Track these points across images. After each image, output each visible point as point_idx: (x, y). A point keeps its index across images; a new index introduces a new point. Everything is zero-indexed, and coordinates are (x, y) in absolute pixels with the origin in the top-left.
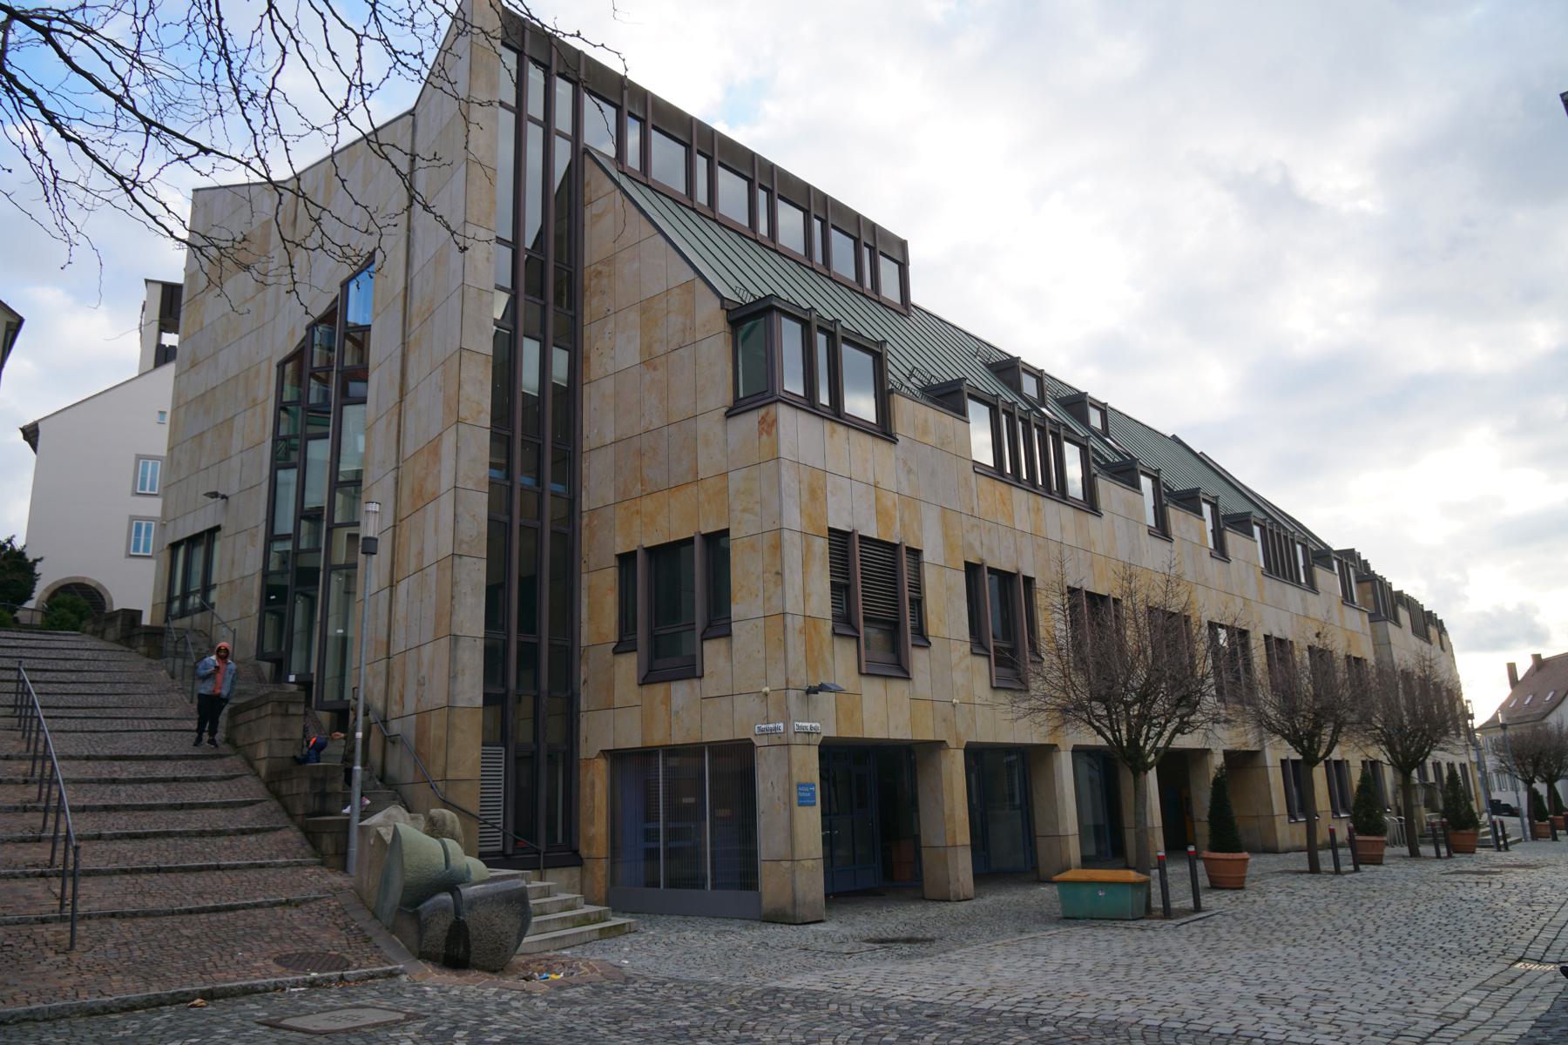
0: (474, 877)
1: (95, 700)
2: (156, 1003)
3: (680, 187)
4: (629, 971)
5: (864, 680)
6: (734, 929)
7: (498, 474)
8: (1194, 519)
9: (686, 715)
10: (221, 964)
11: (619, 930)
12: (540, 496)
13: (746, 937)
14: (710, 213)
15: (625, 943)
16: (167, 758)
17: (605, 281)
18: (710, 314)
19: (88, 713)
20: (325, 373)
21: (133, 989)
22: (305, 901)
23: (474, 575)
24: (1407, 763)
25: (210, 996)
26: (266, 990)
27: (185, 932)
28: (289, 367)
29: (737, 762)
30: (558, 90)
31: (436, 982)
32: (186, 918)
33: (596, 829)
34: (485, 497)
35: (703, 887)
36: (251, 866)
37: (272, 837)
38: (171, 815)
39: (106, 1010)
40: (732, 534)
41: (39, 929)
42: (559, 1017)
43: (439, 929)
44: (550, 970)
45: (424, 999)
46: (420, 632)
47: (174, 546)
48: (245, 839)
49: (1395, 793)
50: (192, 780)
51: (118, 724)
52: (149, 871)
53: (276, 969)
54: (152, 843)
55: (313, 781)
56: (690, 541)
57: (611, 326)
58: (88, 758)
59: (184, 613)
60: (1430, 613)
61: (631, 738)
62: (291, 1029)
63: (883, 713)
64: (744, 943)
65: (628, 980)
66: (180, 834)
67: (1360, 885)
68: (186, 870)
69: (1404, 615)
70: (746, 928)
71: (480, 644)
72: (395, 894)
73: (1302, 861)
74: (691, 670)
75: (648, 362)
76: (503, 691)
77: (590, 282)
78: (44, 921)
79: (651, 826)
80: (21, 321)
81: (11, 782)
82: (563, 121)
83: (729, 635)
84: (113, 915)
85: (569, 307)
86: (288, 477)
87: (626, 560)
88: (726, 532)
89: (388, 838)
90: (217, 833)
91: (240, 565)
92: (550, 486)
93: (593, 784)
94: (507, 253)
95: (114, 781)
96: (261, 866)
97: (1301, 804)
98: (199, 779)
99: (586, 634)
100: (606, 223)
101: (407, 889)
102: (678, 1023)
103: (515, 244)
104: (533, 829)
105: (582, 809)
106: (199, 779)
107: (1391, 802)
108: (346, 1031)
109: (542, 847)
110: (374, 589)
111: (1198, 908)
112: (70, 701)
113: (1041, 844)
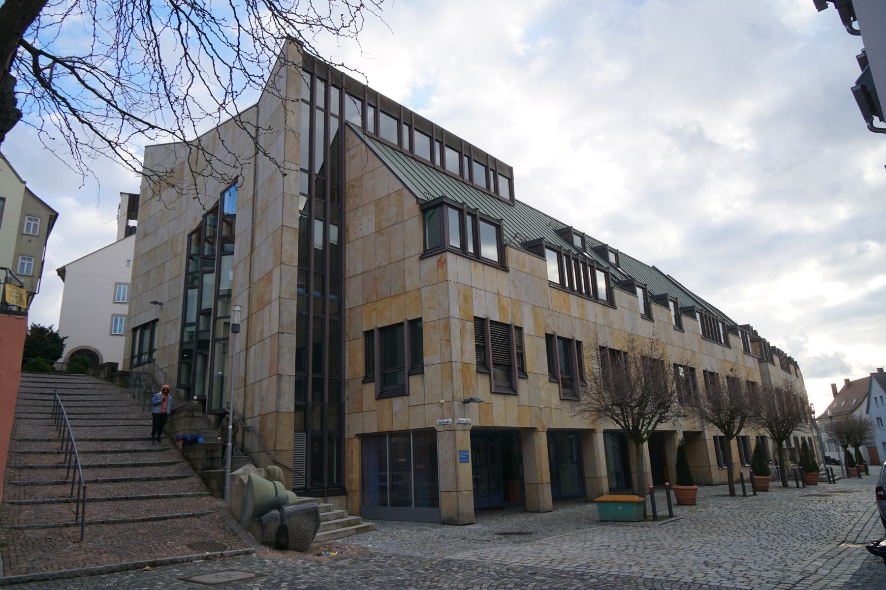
0: (291, 501)
2: (125, 569)
4: (372, 551)
5: (493, 396)
7: (302, 290)
9: (400, 415)
11: (366, 529)
13: (433, 532)
14: (410, 154)
15: (370, 536)
16: (131, 440)
18: (411, 205)
20: (212, 239)
22: (203, 514)
23: (290, 343)
24: (780, 437)
25: (153, 565)
26: (183, 562)
27: (141, 531)
28: (194, 236)
31: (271, 557)
32: (141, 524)
33: (354, 475)
34: (295, 302)
35: (410, 506)
36: (174, 496)
37: (185, 481)
38: (133, 469)
39: (100, 572)
41: (65, 530)
42: (336, 575)
43: (272, 528)
44: (330, 550)
45: (265, 566)
46: (262, 373)
47: (135, 330)
48: (171, 482)
49: (774, 453)
51: (106, 423)
52: (122, 499)
53: (187, 550)
54: (123, 484)
55: (207, 451)
56: (402, 324)
57: (360, 213)
58: (90, 440)
59: (139, 364)
60: (790, 358)
62: (195, 582)
63: (504, 413)
64: (432, 535)
65: (371, 555)
66: (138, 480)
67: (757, 502)
69: (776, 359)
71: (293, 379)
72: (249, 511)
73: (725, 490)
74: (403, 392)
75: (379, 231)
78: (67, 526)
80: (57, 215)
81: (51, 453)
82: (334, 108)
83: (423, 373)
84: (103, 522)
85: (338, 204)
86: (193, 293)
87: (369, 334)
88: (420, 319)
89: (246, 481)
90: (157, 479)
91: (168, 338)
92: (329, 296)
93: (352, 452)
95: (104, 452)
96: (180, 496)
97: (724, 459)
99: (348, 373)
102: (398, 578)
103: (310, 172)
104: (321, 473)
105: (347, 465)
107: (772, 458)
108: (225, 583)
109: (326, 485)
110: (238, 351)
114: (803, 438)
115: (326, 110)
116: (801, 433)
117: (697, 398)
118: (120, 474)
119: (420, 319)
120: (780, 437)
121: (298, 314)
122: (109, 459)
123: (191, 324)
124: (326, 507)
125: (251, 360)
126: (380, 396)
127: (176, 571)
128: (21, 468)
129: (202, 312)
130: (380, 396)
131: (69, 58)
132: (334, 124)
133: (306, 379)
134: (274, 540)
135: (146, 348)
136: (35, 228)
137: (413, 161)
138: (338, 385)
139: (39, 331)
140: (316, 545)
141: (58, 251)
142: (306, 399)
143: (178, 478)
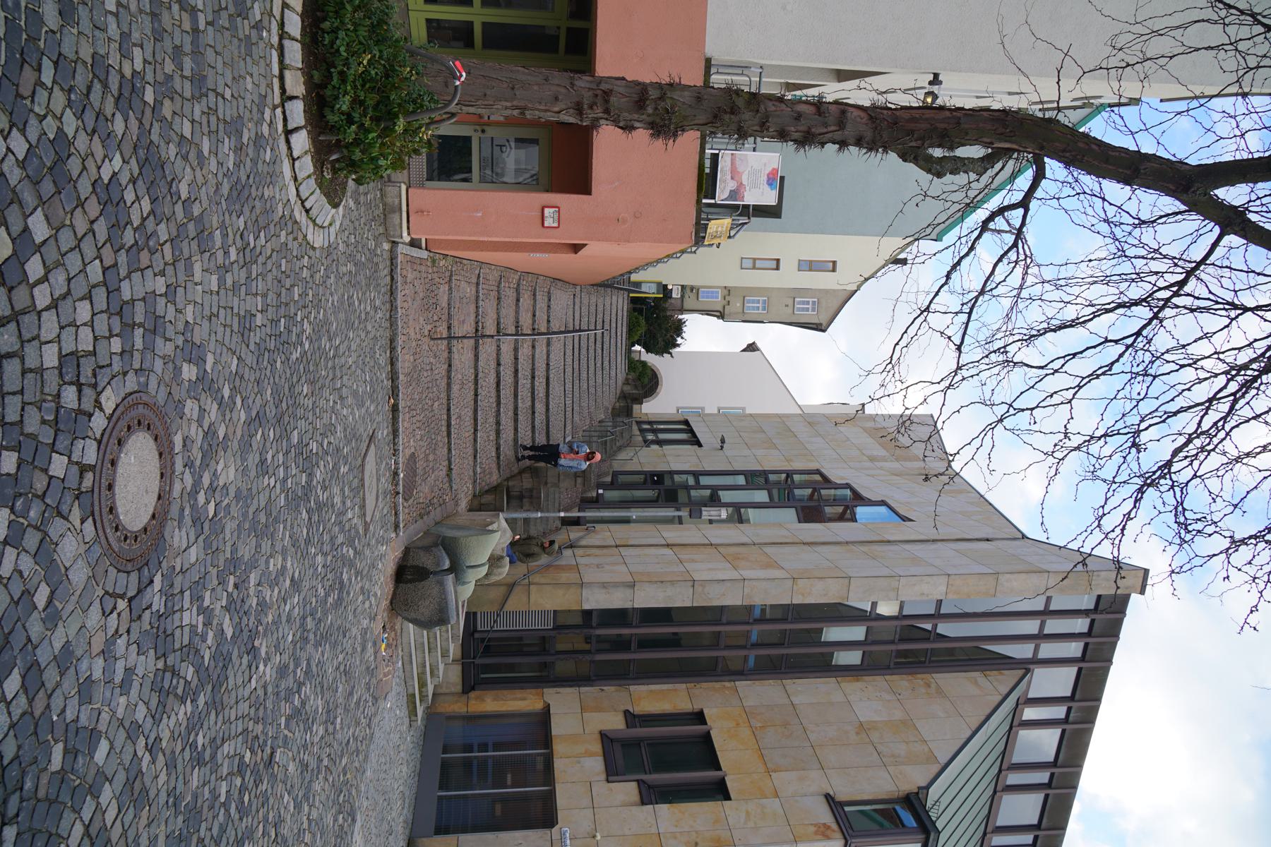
0: (460, 588)
1: (584, 375)
2: (393, 377)
4: (381, 703)
6: (405, 811)
7: (757, 613)
9: (577, 770)
10: (414, 420)
11: (413, 712)
12: (743, 647)
13: (398, 816)
14: (1000, 789)
15: (402, 712)
16: (548, 410)
17: (923, 691)
18: (913, 778)
19: (576, 346)
20: (817, 500)
21: (404, 365)
22: (450, 481)
23: (680, 598)
25: (395, 409)
26: (395, 444)
27: (436, 404)
28: (818, 477)
29: (569, 29)
30: (1074, 644)
31: (388, 556)
32: (445, 407)
33: (490, 703)
34: (739, 603)
35: (441, 788)
36: (476, 451)
37: (494, 466)
38: (511, 407)
39: (393, 349)
40: (727, 803)
41: (445, 325)
42: (354, 631)
43: (426, 561)
44: (388, 646)
45: (378, 542)
46: (632, 567)
47: (686, 422)
48: (494, 449)
50: (533, 422)
51: (569, 386)
52: (476, 390)
53: (408, 452)
54: (493, 393)
55: (531, 490)
56: (719, 768)
57: (887, 697)
58: (548, 364)
59: (642, 431)
61: (560, 726)
62: (368, 446)
64: (394, 814)
65: (376, 699)
66: (498, 411)
68: (476, 411)
70: (405, 822)
71: (628, 605)
72: (450, 533)
74: (613, 772)
75: (862, 728)
76: (594, 625)
77: (920, 679)
78: (449, 328)
79: (490, 747)
80: (824, 331)
81: (534, 321)
82: (1048, 650)
83: (643, 803)
84: (450, 366)
85: (896, 663)
86: (741, 480)
87: (699, 717)
88: (728, 798)
89: (490, 528)
90: (498, 433)
91: (678, 459)
92: (752, 655)
93: (524, 699)
94: (931, 610)
95: (533, 377)
96: (475, 457)
98: (533, 427)
99: (639, 690)
100: (970, 690)
101: (454, 539)
102: (339, 720)
103: (938, 616)
104: (494, 654)
105: (505, 692)
106: (533, 427)
108: (362, 480)
109: (478, 661)
110: (665, 534)
112: (584, 362)
115: (1041, 637)
118: (507, 392)
119: (728, 798)
121: (722, 609)
122: (524, 382)
123: (697, 481)
124: (448, 651)
125: (652, 551)
126: (605, 738)
127: (384, 433)
128: (518, 291)
129: (715, 489)
130: (605, 738)
131: (1025, 242)
132: (1022, 651)
133: (629, 625)
134: (410, 563)
135: (662, 436)
136: (803, 309)
137: (989, 792)
138: (621, 674)
139: (678, 328)
140: (398, 627)
141: (778, 340)
142: (601, 625)
143: (498, 458)
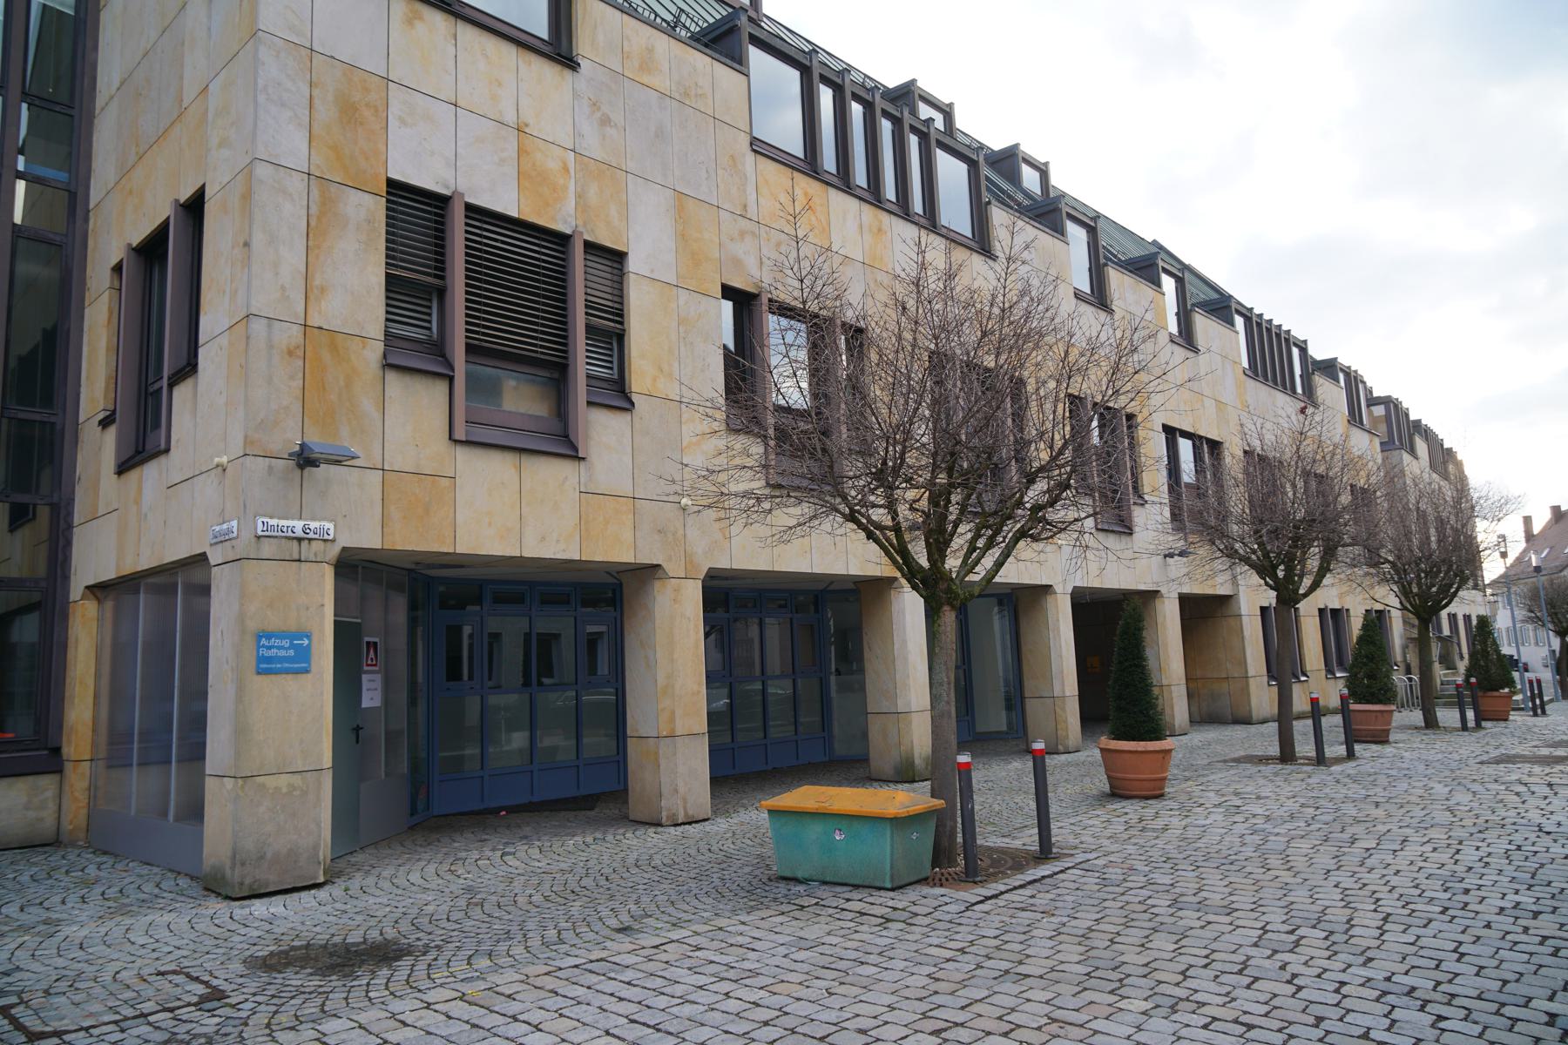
3: (796, 147)
5: (462, 454)
8: (1146, 290)
24: (1425, 609)
49: (1405, 648)
60: (1450, 450)
63: (508, 512)
67: (1357, 791)
69: (1421, 446)
73: (1265, 740)
97: (1283, 664)
107: (1399, 658)
111: (1045, 852)
113: (1031, 705)
114: (1467, 618)
116: (1467, 605)
117: (1223, 516)
120: (1425, 609)
